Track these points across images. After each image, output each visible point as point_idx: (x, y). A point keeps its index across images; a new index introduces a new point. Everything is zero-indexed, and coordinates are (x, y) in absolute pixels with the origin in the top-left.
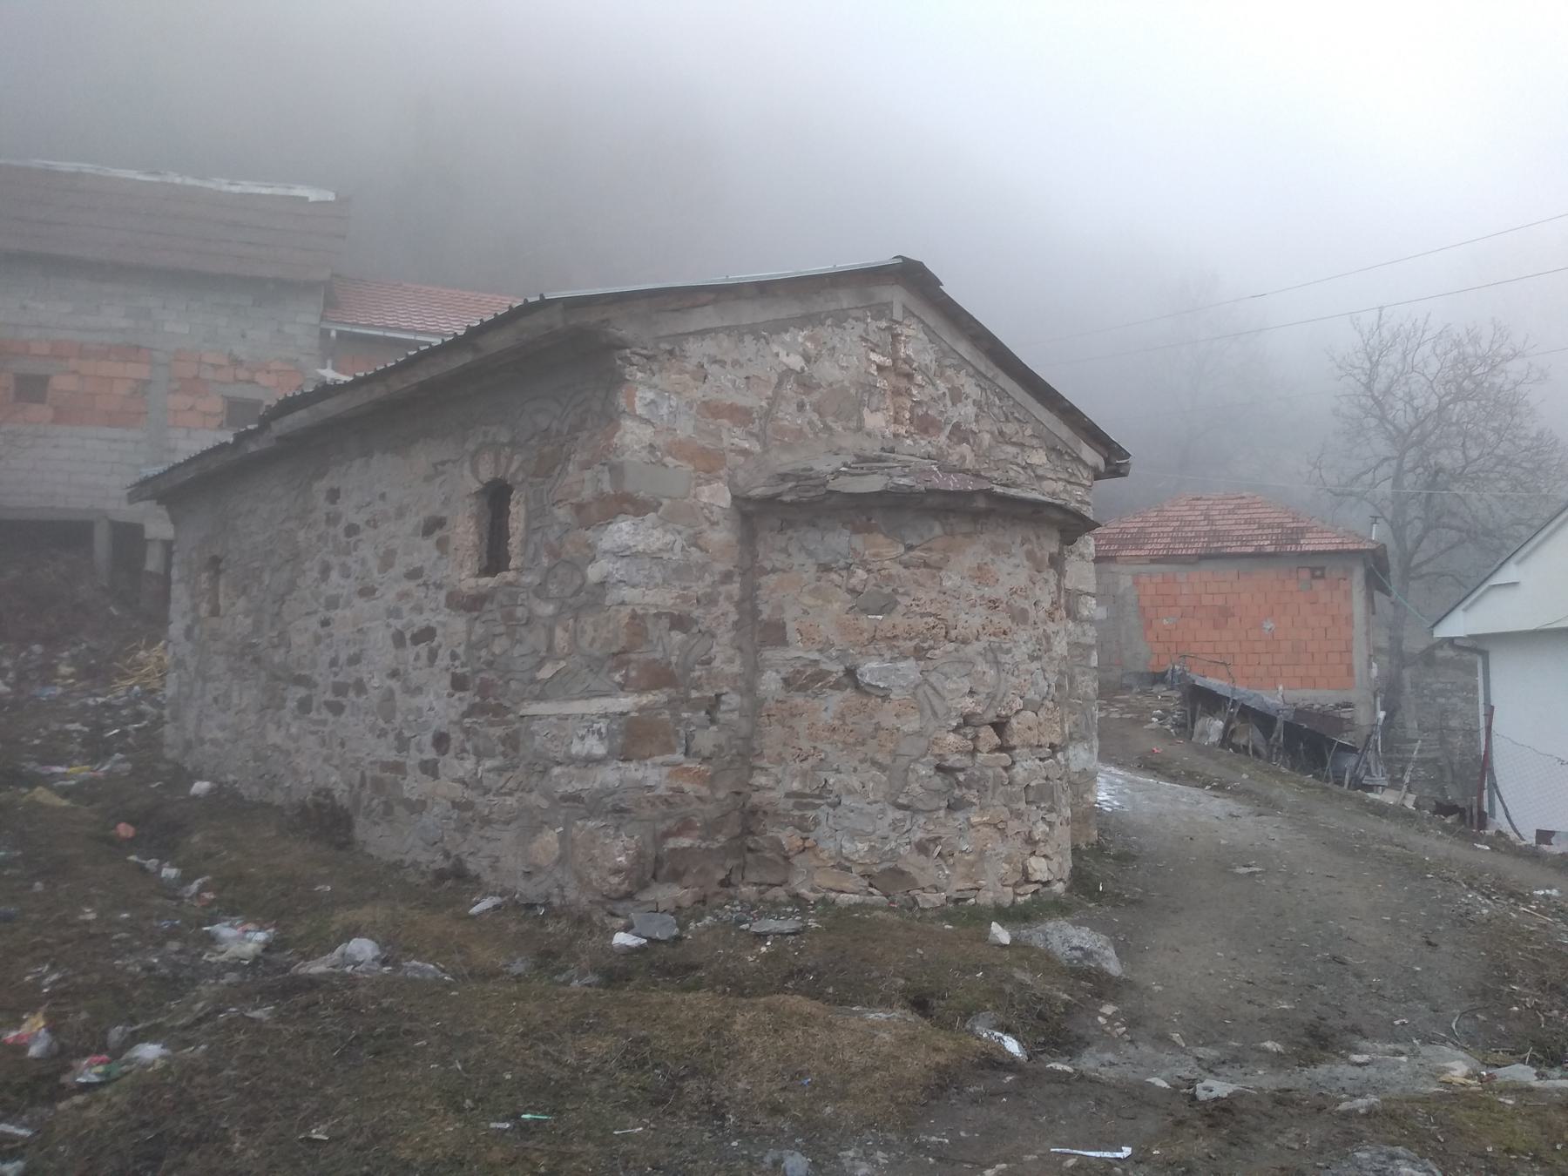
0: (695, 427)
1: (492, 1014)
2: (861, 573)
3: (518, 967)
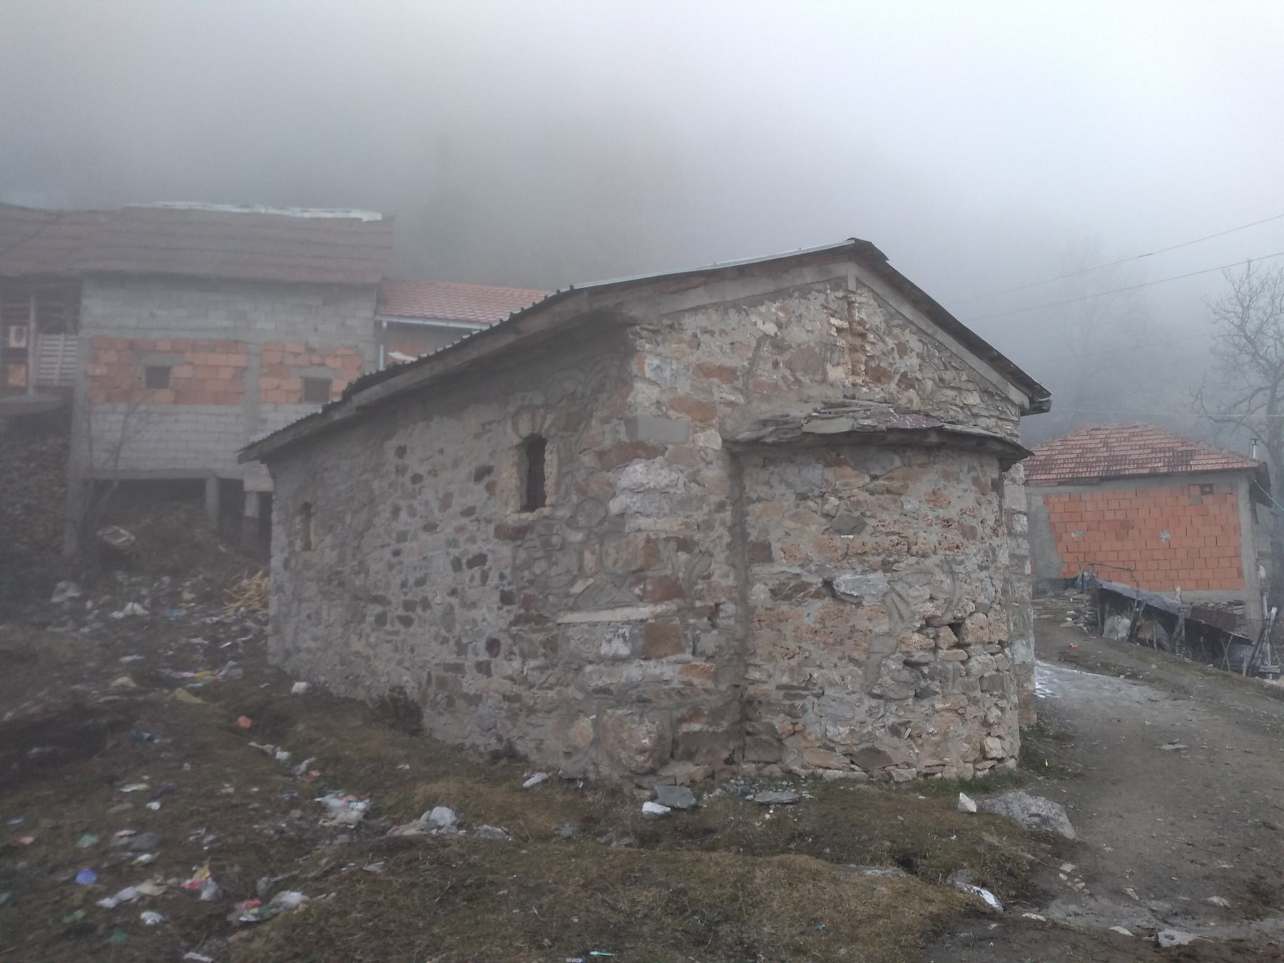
0: (692, 386)
1: (558, 868)
2: (833, 500)
3: (567, 830)
